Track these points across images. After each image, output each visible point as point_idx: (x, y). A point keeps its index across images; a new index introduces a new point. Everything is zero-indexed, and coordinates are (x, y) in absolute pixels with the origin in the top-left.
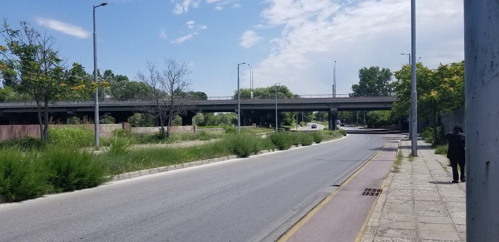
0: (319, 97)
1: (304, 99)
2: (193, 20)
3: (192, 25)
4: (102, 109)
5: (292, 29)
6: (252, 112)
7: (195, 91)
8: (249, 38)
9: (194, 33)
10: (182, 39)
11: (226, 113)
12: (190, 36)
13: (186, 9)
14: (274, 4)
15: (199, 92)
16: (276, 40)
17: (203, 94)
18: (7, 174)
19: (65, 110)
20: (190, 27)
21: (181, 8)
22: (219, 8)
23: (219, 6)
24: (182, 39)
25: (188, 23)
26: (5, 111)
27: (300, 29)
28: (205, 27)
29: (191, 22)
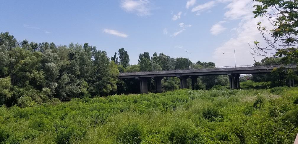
0: (230, 67)
1: (221, 69)
2: (183, 23)
3: (182, 25)
4: (203, 73)
5: (245, 21)
6: (236, 75)
7: (208, 62)
8: (216, 29)
9: (184, 30)
10: (176, 34)
11: (245, 75)
12: (181, 31)
13: (179, 17)
14: (233, 8)
15: (210, 63)
16: (235, 29)
17: (213, 63)
18: (171, 139)
19: (134, 77)
20: (181, 26)
21: (177, 16)
22: (198, 14)
23: (198, 13)
24: (176, 34)
25: (180, 24)
26: (141, 77)
27: (251, 21)
28: (190, 26)
29: (182, 24)
